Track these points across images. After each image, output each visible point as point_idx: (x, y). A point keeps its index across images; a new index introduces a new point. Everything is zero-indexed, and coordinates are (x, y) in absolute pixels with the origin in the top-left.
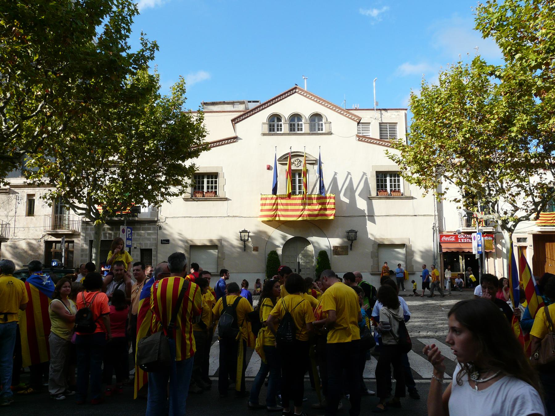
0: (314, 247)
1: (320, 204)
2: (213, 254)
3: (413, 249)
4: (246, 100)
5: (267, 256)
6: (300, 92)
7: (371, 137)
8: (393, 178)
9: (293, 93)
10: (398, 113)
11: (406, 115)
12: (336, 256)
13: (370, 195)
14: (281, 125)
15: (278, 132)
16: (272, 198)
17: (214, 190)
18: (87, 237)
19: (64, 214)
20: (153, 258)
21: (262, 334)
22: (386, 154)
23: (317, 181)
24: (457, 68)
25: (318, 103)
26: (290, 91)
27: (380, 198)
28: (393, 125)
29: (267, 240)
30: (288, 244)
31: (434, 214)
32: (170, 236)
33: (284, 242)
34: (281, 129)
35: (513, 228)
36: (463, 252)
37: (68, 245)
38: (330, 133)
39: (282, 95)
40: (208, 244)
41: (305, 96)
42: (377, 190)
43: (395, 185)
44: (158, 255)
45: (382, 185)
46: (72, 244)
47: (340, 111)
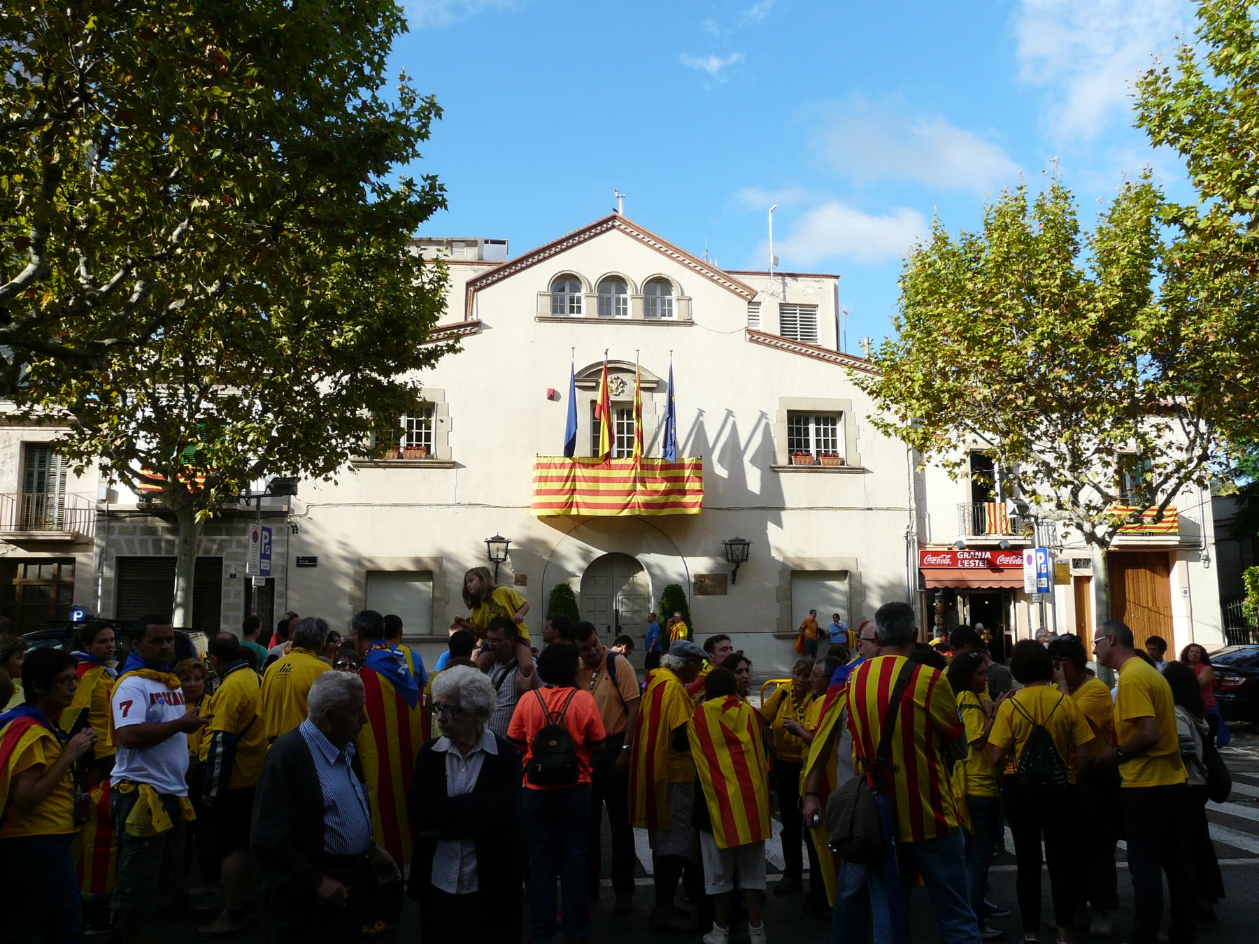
0: (652, 575)
1: (667, 479)
2: (420, 592)
3: (867, 581)
4: (480, 236)
5: (547, 595)
6: (623, 227)
7: (762, 330)
8: (822, 427)
9: (608, 230)
10: (819, 285)
11: (836, 288)
12: (700, 597)
13: (775, 462)
14: (579, 301)
15: (572, 315)
16: (562, 466)
17: (423, 443)
18: (109, 550)
19: (48, 491)
20: (276, 600)
21: (961, 769)
22: (849, 375)
23: (659, 427)
24: (1016, 199)
25: (664, 253)
26: (601, 224)
27: (797, 470)
28: (809, 310)
29: (547, 558)
30: (594, 569)
31: (907, 507)
32: (319, 548)
33: (585, 565)
34: (579, 308)
35: (1107, 539)
36: (969, 588)
37: (59, 567)
38: (689, 323)
39: (583, 232)
40: (410, 567)
41: (635, 238)
42: (790, 452)
43: (826, 442)
44: (290, 593)
45: (799, 441)
46: (70, 567)
47: (710, 274)
